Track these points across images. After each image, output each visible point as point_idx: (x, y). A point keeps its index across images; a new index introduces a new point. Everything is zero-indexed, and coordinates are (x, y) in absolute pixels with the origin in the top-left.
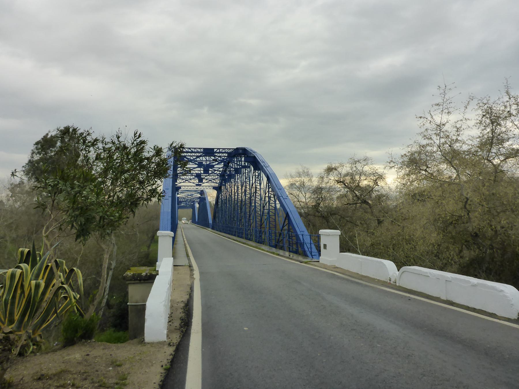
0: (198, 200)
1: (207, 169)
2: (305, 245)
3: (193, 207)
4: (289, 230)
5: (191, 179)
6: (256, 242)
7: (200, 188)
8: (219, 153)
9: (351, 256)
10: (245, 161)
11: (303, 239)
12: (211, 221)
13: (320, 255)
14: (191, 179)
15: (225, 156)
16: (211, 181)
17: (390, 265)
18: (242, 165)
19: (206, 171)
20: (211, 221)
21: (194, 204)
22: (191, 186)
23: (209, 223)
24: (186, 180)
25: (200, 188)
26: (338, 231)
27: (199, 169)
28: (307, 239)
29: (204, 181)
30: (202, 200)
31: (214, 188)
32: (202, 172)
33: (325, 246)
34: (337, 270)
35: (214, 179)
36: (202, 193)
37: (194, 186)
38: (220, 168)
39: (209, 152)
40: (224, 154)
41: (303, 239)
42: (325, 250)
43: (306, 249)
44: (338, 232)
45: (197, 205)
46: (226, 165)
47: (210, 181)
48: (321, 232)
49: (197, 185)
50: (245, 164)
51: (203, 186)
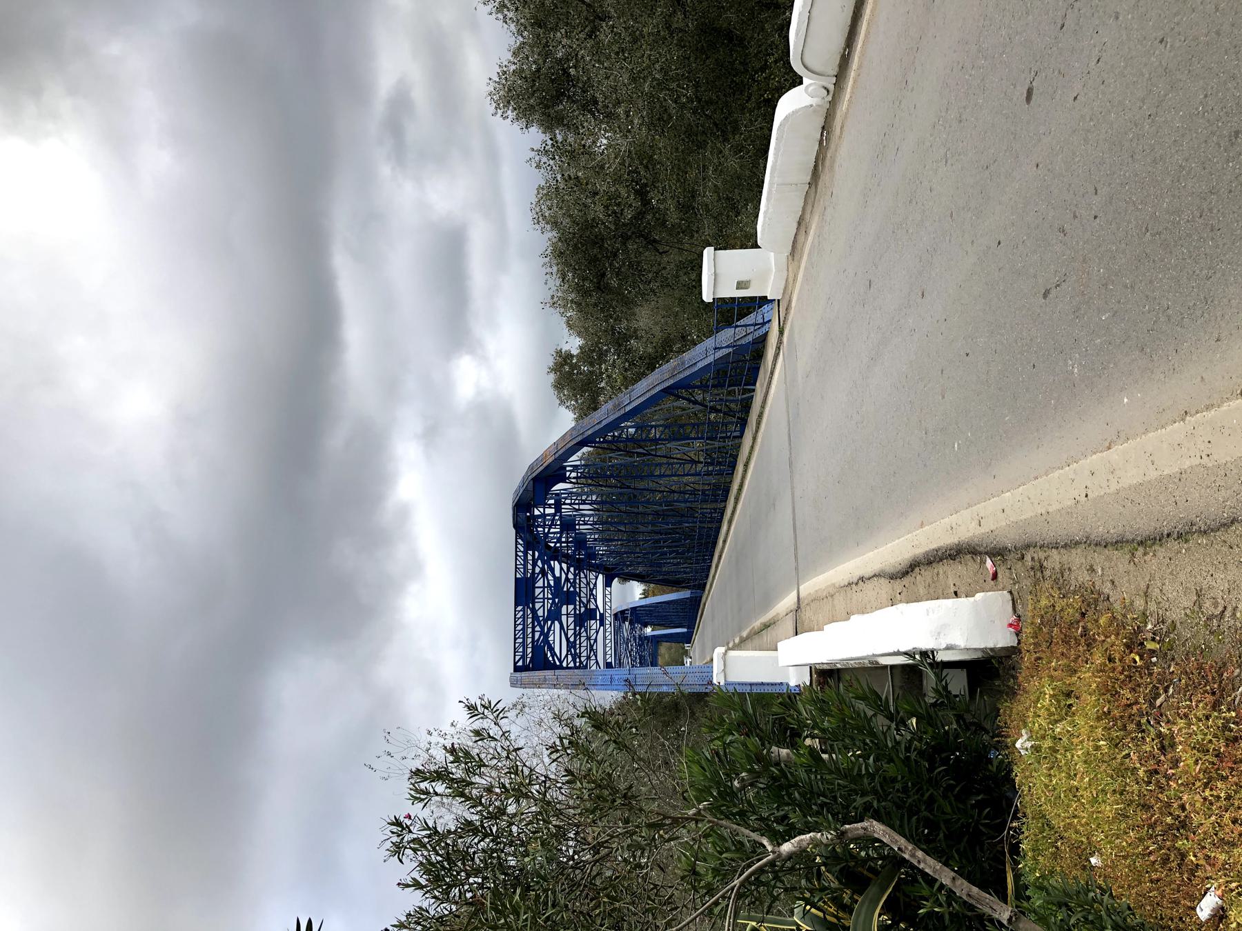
0: (638, 626)
1: (564, 596)
2: (743, 342)
3: (656, 640)
4: (704, 387)
5: (588, 584)
6: (741, 436)
7: (609, 619)
8: (525, 566)
9: (765, 212)
10: (545, 505)
11: (728, 347)
12: (685, 594)
13: (764, 300)
14: (588, 638)
15: (533, 555)
16: (591, 590)
17: (789, 104)
18: (554, 515)
19: (569, 598)
20: (685, 594)
21: (647, 638)
22: (605, 638)
23: (690, 599)
24: (592, 649)
25: (609, 619)
26: (706, 252)
27: (564, 618)
28: (726, 336)
29: (593, 607)
30: (635, 616)
31: (608, 583)
32: (571, 607)
33: (741, 285)
34: (791, 280)
35: (588, 584)
36: (620, 616)
37: (605, 631)
38: (561, 569)
39: (524, 592)
40: (530, 557)
41: (728, 347)
42: (752, 284)
43: (750, 338)
44: (708, 253)
45: (648, 631)
46: (556, 554)
47: (592, 649)
48: (707, 297)
49: (602, 623)
50: (550, 506)
51: (605, 609)
